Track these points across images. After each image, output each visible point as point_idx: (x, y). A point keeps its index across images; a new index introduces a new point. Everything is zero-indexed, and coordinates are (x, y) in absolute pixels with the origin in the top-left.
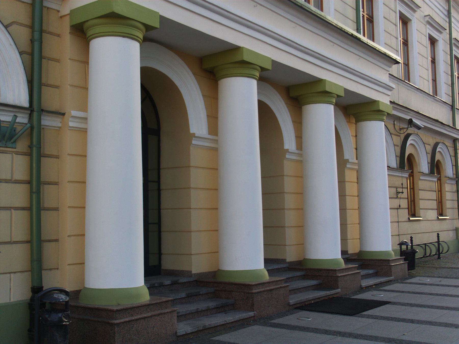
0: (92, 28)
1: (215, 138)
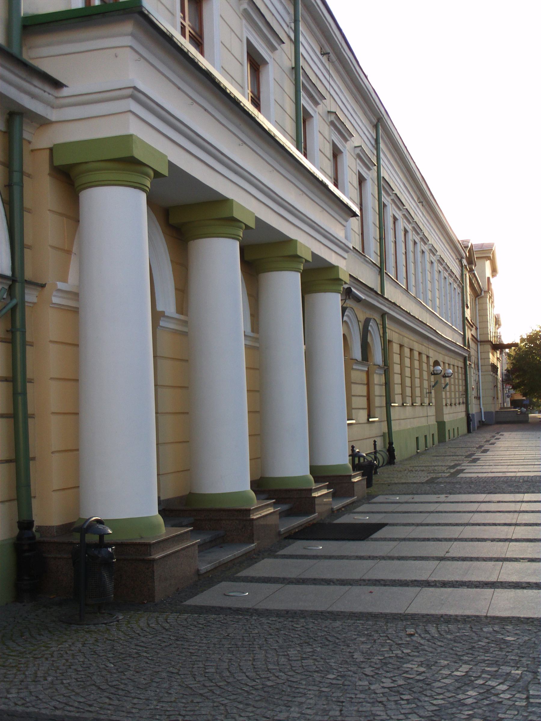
0: (90, 173)
1: (182, 317)
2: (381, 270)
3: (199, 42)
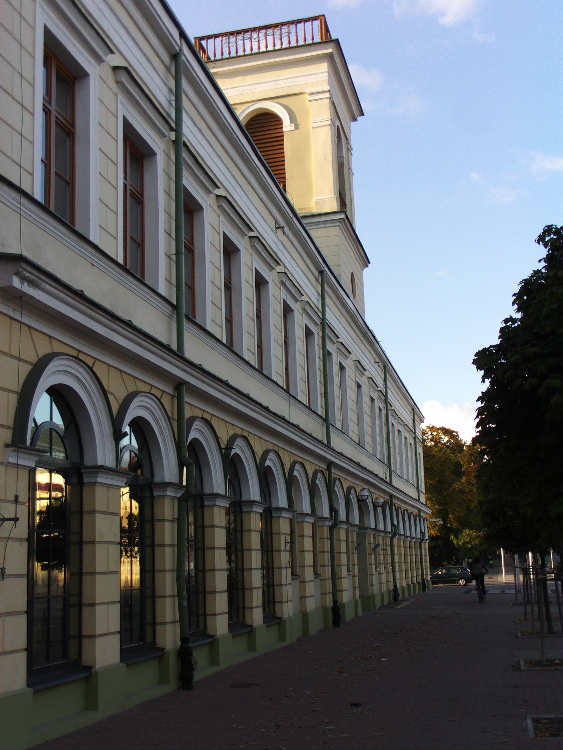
2: (326, 421)
3: (71, 131)
